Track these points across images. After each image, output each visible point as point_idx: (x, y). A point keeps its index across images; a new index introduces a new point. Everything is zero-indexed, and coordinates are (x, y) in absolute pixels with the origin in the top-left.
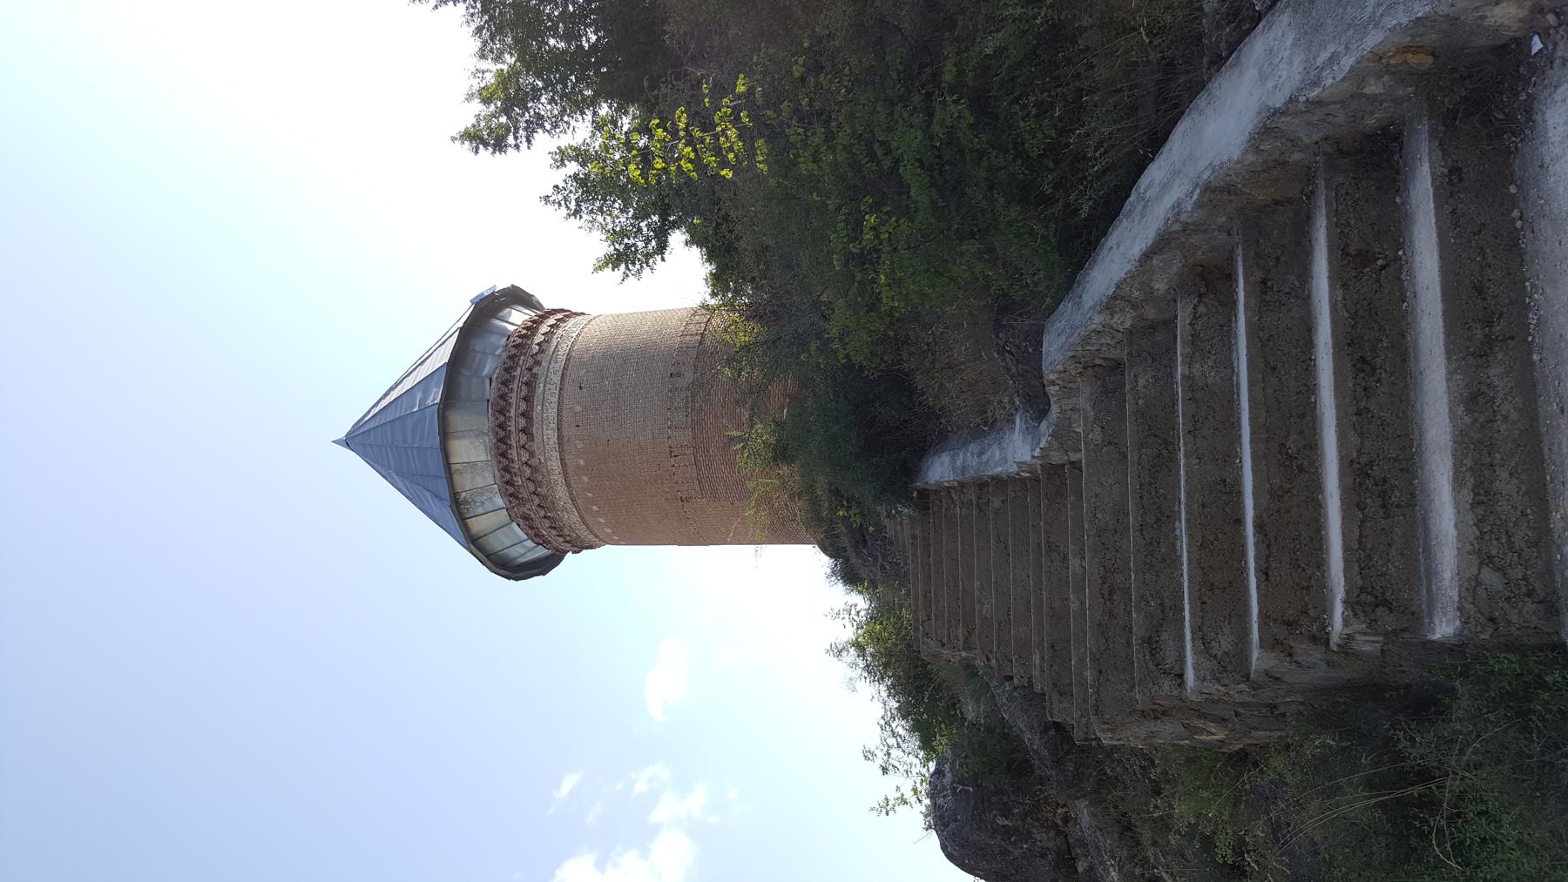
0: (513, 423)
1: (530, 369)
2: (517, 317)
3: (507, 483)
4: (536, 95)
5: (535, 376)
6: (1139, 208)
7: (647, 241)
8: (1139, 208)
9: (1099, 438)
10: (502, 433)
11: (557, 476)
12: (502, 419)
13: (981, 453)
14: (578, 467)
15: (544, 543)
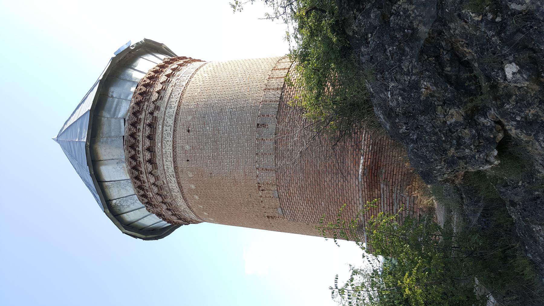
0: (141, 156)
1: (152, 113)
2: (145, 65)
5: (155, 119)
10: (134, 163)
14: (190, 189)
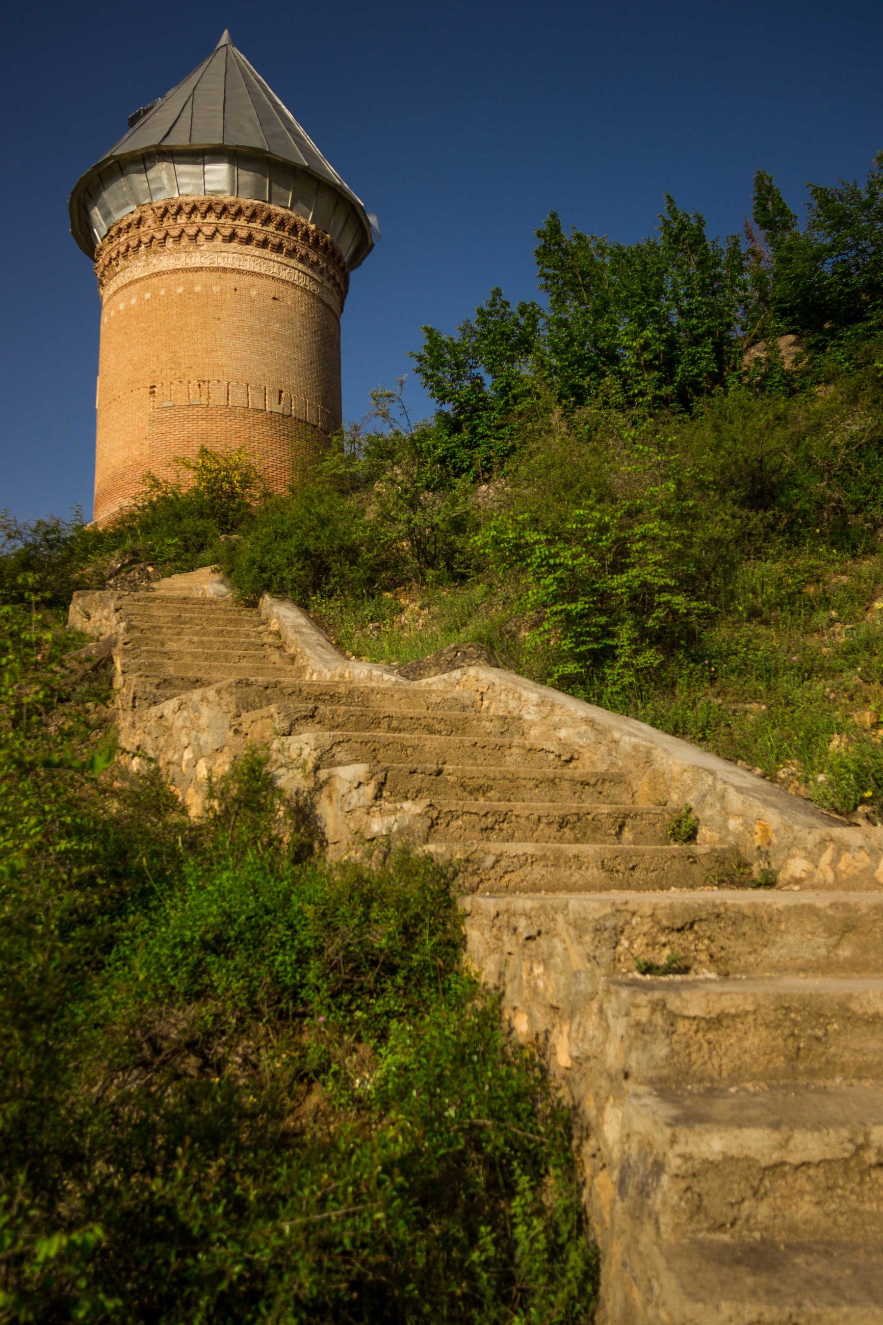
4: (344, 876)
11: (184, 260)
14: (193, 284)
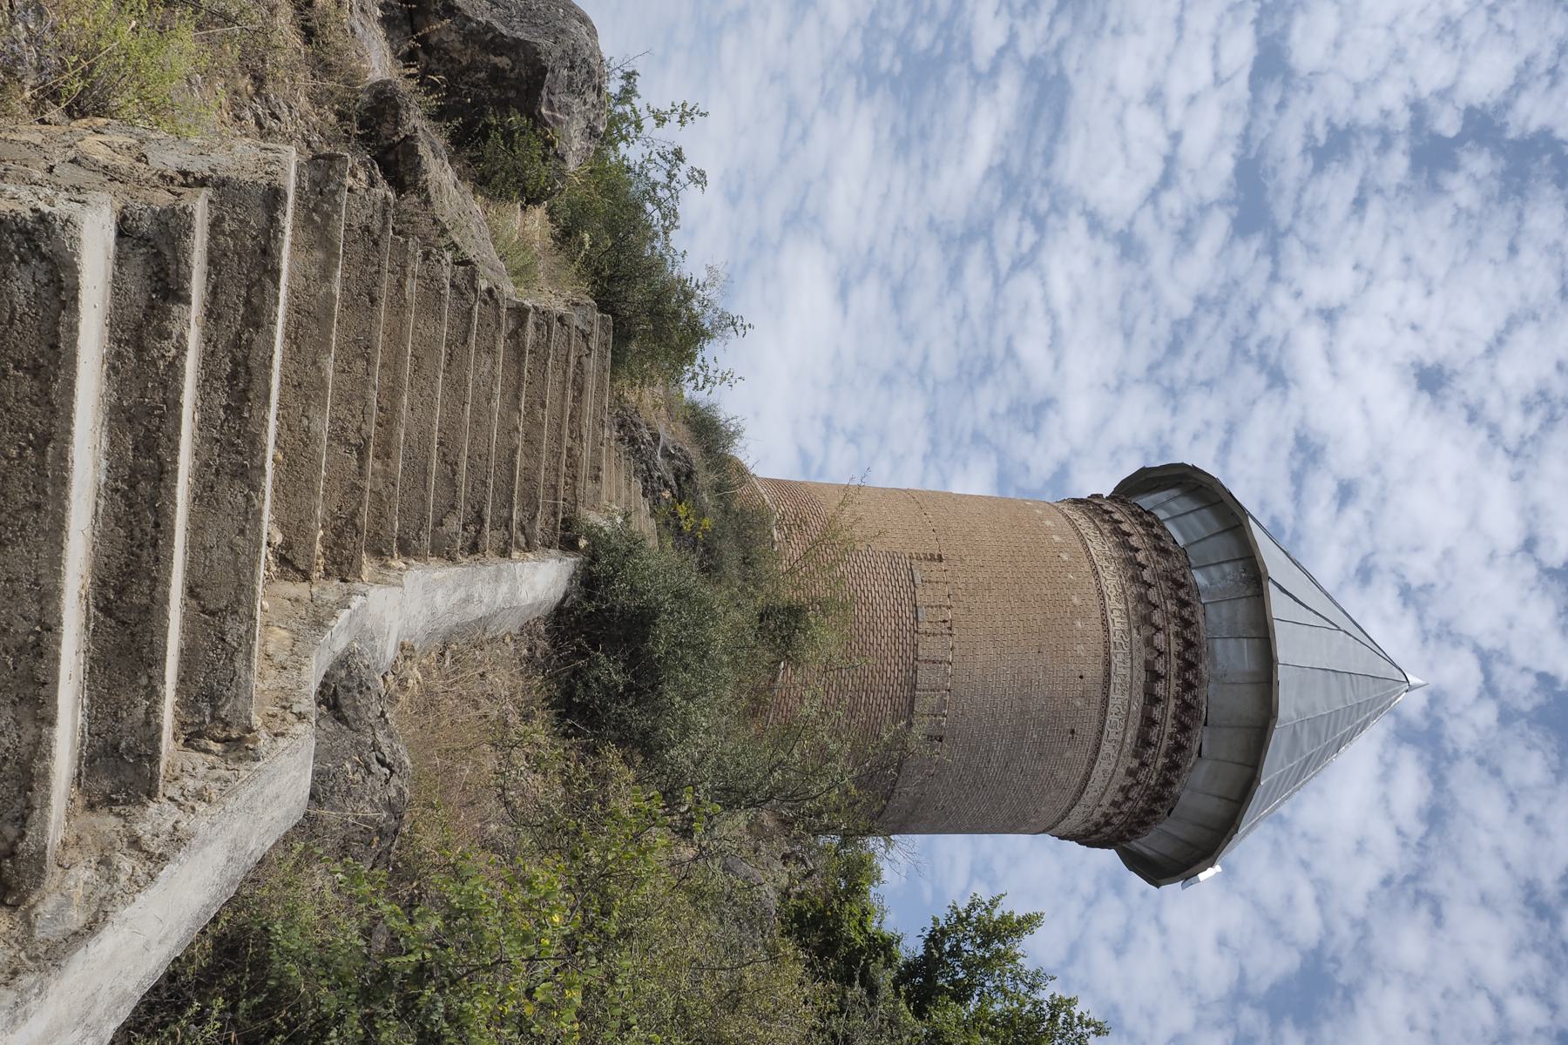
3: (1182, 586)
5: (1136, 755)
6: (98, 1011)
7: (956, 952)
8: (98, 1011)
9: (229, 623)
10: (1189, 676)
12: (1188, 697)
13: (467, 600)
15: (1141, 515)
